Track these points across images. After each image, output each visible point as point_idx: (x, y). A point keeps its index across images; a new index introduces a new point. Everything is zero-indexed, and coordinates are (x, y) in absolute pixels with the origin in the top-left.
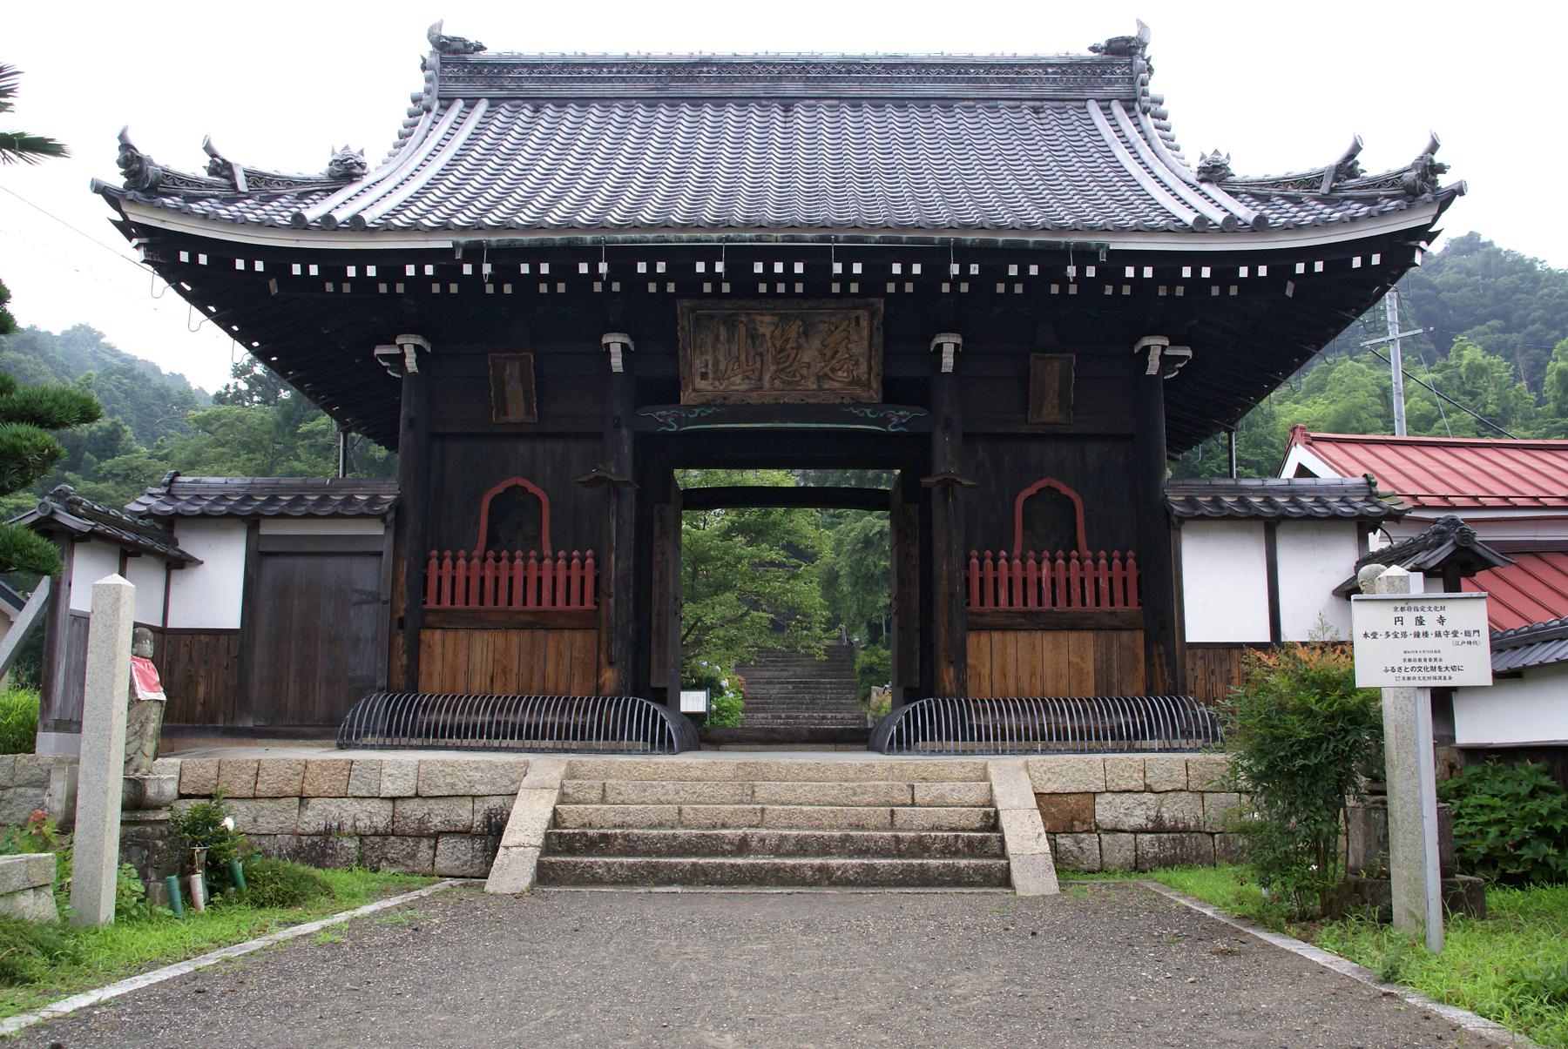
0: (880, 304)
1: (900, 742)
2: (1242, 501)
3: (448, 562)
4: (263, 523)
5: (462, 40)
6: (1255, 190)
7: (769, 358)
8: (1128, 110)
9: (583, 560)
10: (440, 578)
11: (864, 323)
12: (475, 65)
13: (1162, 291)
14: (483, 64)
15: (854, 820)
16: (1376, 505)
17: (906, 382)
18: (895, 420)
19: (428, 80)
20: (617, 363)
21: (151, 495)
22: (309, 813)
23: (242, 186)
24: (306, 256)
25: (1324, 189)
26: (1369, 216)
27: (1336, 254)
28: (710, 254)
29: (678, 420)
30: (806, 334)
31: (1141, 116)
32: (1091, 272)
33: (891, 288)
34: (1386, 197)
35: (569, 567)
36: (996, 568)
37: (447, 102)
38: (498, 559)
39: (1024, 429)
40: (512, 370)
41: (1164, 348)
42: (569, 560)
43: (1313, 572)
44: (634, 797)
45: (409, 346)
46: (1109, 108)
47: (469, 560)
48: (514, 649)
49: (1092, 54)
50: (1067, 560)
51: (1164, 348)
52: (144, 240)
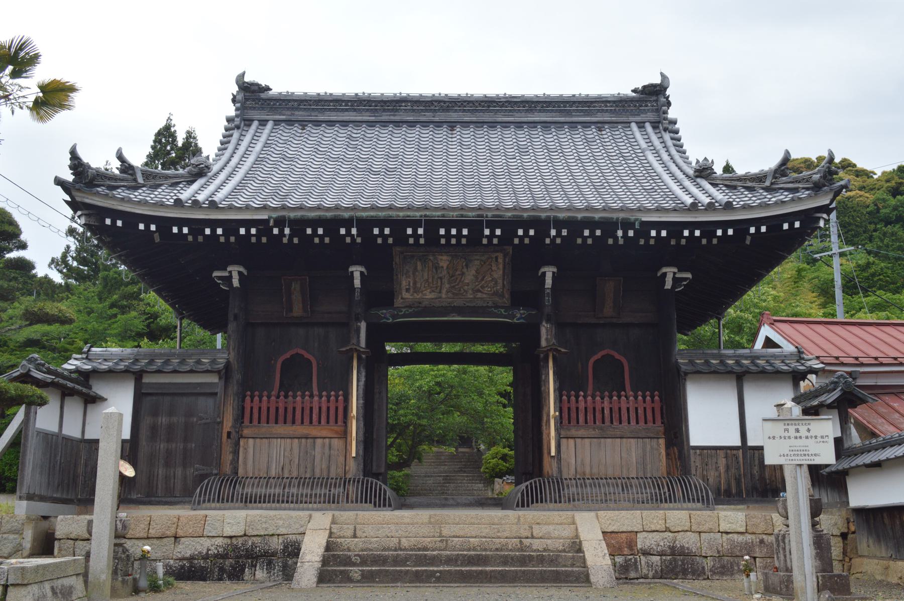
0: (510, 249)
2: (722, 362)
3: (256, 398)
4: (144, 375)
5: (258, 85)
6: (727, 183)
7: (445, 281)
8: (654, 128)
9: (337, 397)
10: (252, 408)
11: (500, 260)
12: (265, 100)
13: (673, 242)
15: (499, 546)
16: (803, 365)
17: (525, 293)
18: (518, 315)
19: (237, 109)
20: (357, 283)
21: (76, 359)
22: (180, 546)
23: (140, 180)
24: (181, 222)
25: (767, 183)
26: (793, 200)
27: (774, 222)
28: (415, 224)
29: (394, 317)
30: (467, 266)
31: (663, 132)
32: (631, 233)
33: (516, 241)
34: (803, 188)
35: (328, 401)
36: (577, 402)
37: (248, 122)
38: (286, 397)
39: (594, 321)
40: (296, 287)
41: (675, 273)
42: (328, 397)
43: (766, 403)
44: (372, 534)
45: (235, 271)
46: (644, 127)
47: (269, 397)
48: (296, 451)
49: (634, 94)
50: (619, 397)
51: (675, 273)
52: (86, 212)
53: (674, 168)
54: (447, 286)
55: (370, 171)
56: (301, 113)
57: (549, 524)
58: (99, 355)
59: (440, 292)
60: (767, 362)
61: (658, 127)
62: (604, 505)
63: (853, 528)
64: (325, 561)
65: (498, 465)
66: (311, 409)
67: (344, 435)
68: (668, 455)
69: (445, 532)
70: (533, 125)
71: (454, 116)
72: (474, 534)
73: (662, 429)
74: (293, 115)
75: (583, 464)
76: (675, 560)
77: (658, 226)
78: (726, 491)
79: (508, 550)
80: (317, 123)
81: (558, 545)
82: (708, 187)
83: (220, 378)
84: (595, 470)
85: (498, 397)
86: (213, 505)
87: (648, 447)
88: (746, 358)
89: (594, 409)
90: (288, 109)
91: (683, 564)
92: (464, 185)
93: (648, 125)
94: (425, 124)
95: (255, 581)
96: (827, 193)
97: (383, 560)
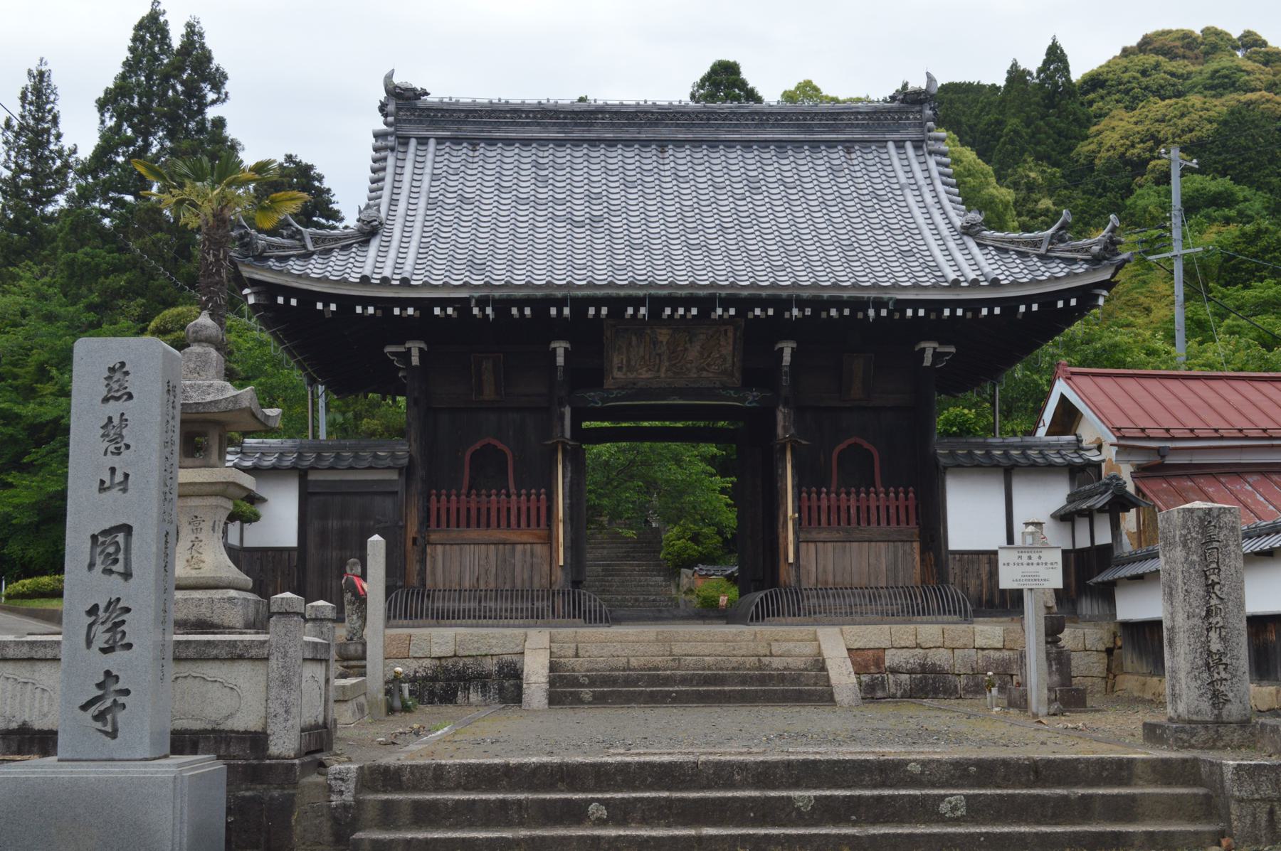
1: (757, 618)
6: (998, 245)
9: (538, 495)
10: (438, 509)
11: (730, 334)
12: (423, 110)
14: (429, 109)
16: (1080, 456)
17: (758, 370)
18: (751, 398)
20: (560, 360)
23: (311, 247)
26: (1068, 275)
27: (1047, 300)
30: (691, 341)
32: (884, 313)
35: (528, 500)
36: (819, 499)
37: (404, 141)
45: (415, 348)
46: (903, 147)
47: (458, 496)
50: (868, 493)
52: (255, 289)
53: (938, 218)
54: (667, 364)
55: (573, 222)
56: (469, 127)
57: (788, 641)
58: (255, 449)
59: (658, 371)
60: (1041, 452)
61: (921, 147)
62: (849, 618)
63: (1119, 643)
64: (552, 682)
65: (686, 548)
66: (509, 509)
67: (549, 540)
68: (922, 560)
69: (676, 650)
70: (764, 144)
71: (664, 133)
72: (707, 652)
73: (917, 531)
74: (459, 130)
75: (825, 571)
76: (925, 678)
77: (915, 304)
78: (987, 601)
79: (745, 669)
80: (491, 142)
81: (799, 663)
82: (975, 250)
83: (400, 474)
84: (839, 579)
85: (702, 466)
86: (400, 622)
87: (901, 552)
88: (1016, 448)
89: (839, 507)
90: (453, 122)
91: (934, 682)
92: (688, 245)
93: (908, 145)
94: (628, 143)
95: (470, 704)
96: (1105, 267)
97: (611, 681)
